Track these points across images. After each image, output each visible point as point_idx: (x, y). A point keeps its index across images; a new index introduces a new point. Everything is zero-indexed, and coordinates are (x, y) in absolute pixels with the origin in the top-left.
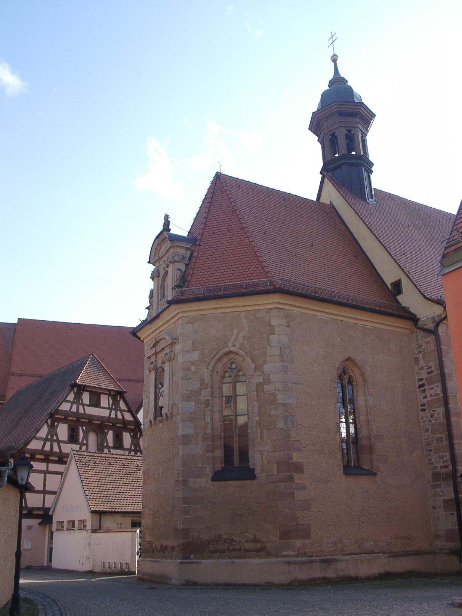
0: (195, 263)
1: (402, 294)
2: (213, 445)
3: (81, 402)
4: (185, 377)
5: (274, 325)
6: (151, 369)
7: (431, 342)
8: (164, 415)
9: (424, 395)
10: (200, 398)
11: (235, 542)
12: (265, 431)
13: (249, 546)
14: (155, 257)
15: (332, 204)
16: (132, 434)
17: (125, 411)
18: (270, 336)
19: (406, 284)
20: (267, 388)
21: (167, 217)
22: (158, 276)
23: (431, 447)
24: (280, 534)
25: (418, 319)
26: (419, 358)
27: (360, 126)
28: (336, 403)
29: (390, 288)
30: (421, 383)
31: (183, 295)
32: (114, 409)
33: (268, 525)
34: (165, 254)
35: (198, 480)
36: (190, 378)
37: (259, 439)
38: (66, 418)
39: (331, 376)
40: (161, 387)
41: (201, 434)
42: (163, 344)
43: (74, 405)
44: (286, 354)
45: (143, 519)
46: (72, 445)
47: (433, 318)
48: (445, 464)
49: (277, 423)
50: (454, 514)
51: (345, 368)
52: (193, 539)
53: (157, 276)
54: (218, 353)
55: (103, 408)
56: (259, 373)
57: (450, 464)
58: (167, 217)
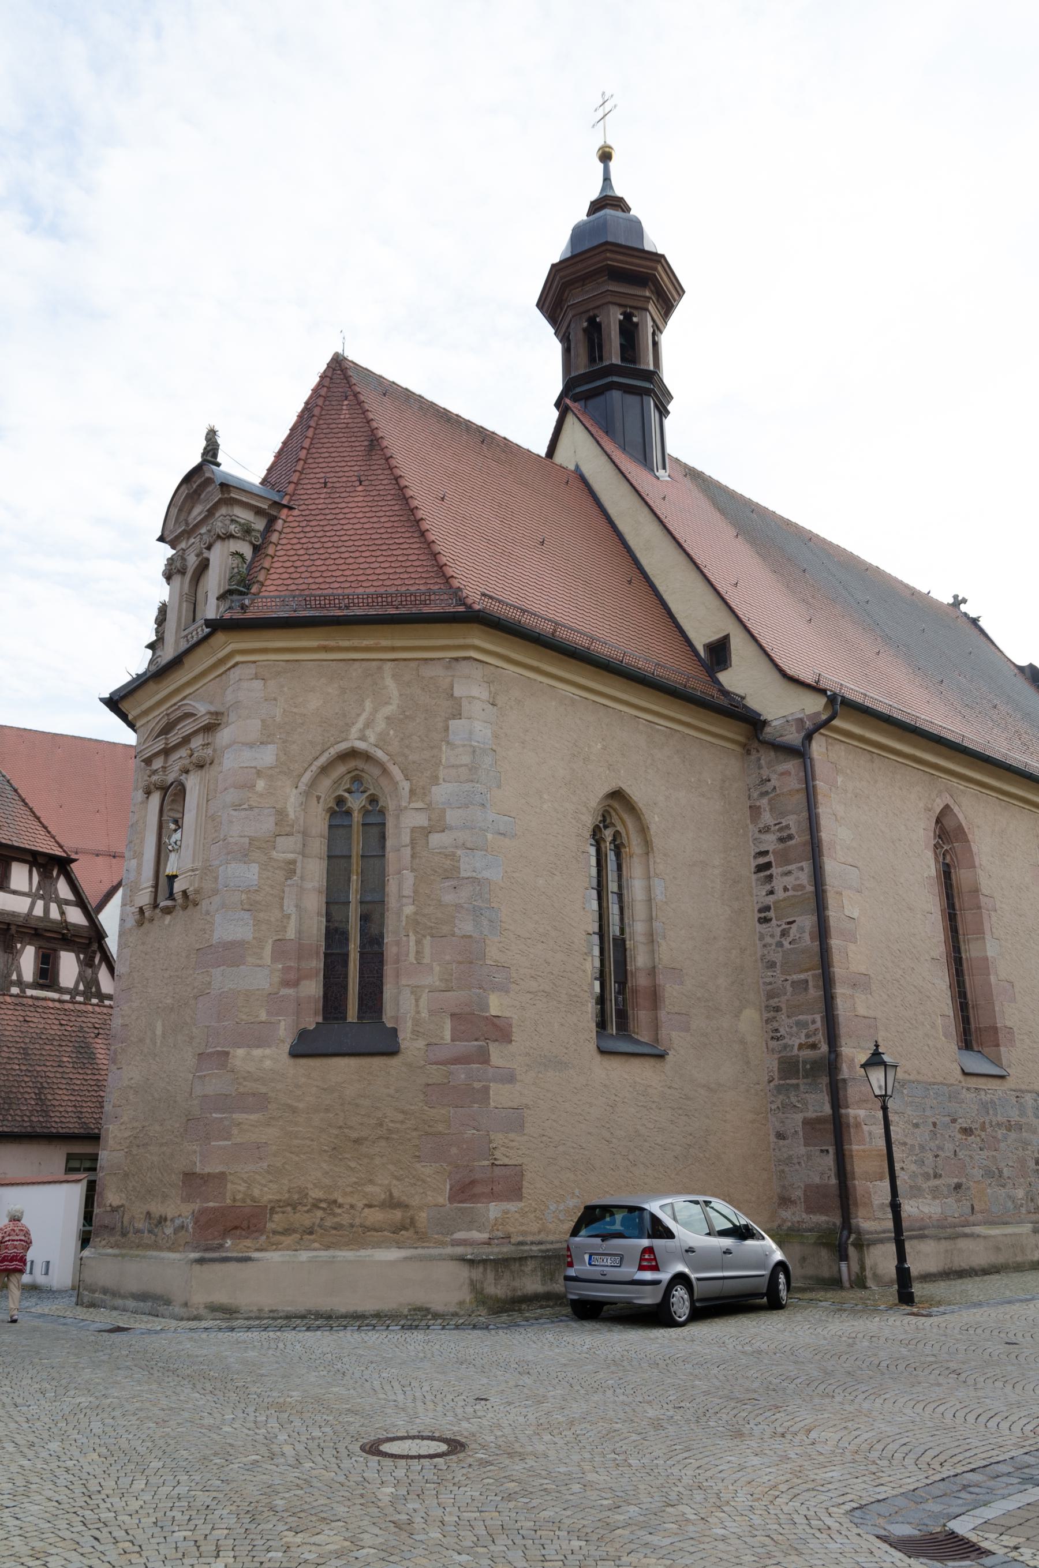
0: (280, 533)
1: (729, 669)
2: (299, 969)
4: (240, 806)
5: (461, 698)
6: (152, 787)
7: (793, 772)
8: (178, 896)
9: (768, 887)
10: (274, 854)
11: (340, 1206)
12: (427, 941)
13: (375, 1216)
14: (177, 525)
15: (580, 470)
16: (82, 956)
17: (67, 902)
18: (451, 722)
19: (739, 646)
20: (435, 839)
21: (211, 437)
22: (182, 572)
23: (779, 1002)
24: (451, 1189)
25: (765, 723)
26: (759, 807)
27: (651, 307)
28: (587, 889)
29: (702, 653)
30: (762, 860)
31: (245, 612)
32: (42, 897)
33: (423, 1166)
34: (202, 520)
35: (257, 1052)
36: (251, 808)
37: (412, 958)
39: (580, 826)
40: (175, 830)
41: (270, 941)
42: (187, 727)
44: (485, 766)
45: (104, 1149)
47: (801, 721)
48: (811, 1040)
49: (456, 921)
50: (827, 1151)
51: (606, 815)
52: (234, 1200)
53: (179, 571)
55: (15, 892)
56: (420, 805)
57: (822, 1040)
58: (211, 437)
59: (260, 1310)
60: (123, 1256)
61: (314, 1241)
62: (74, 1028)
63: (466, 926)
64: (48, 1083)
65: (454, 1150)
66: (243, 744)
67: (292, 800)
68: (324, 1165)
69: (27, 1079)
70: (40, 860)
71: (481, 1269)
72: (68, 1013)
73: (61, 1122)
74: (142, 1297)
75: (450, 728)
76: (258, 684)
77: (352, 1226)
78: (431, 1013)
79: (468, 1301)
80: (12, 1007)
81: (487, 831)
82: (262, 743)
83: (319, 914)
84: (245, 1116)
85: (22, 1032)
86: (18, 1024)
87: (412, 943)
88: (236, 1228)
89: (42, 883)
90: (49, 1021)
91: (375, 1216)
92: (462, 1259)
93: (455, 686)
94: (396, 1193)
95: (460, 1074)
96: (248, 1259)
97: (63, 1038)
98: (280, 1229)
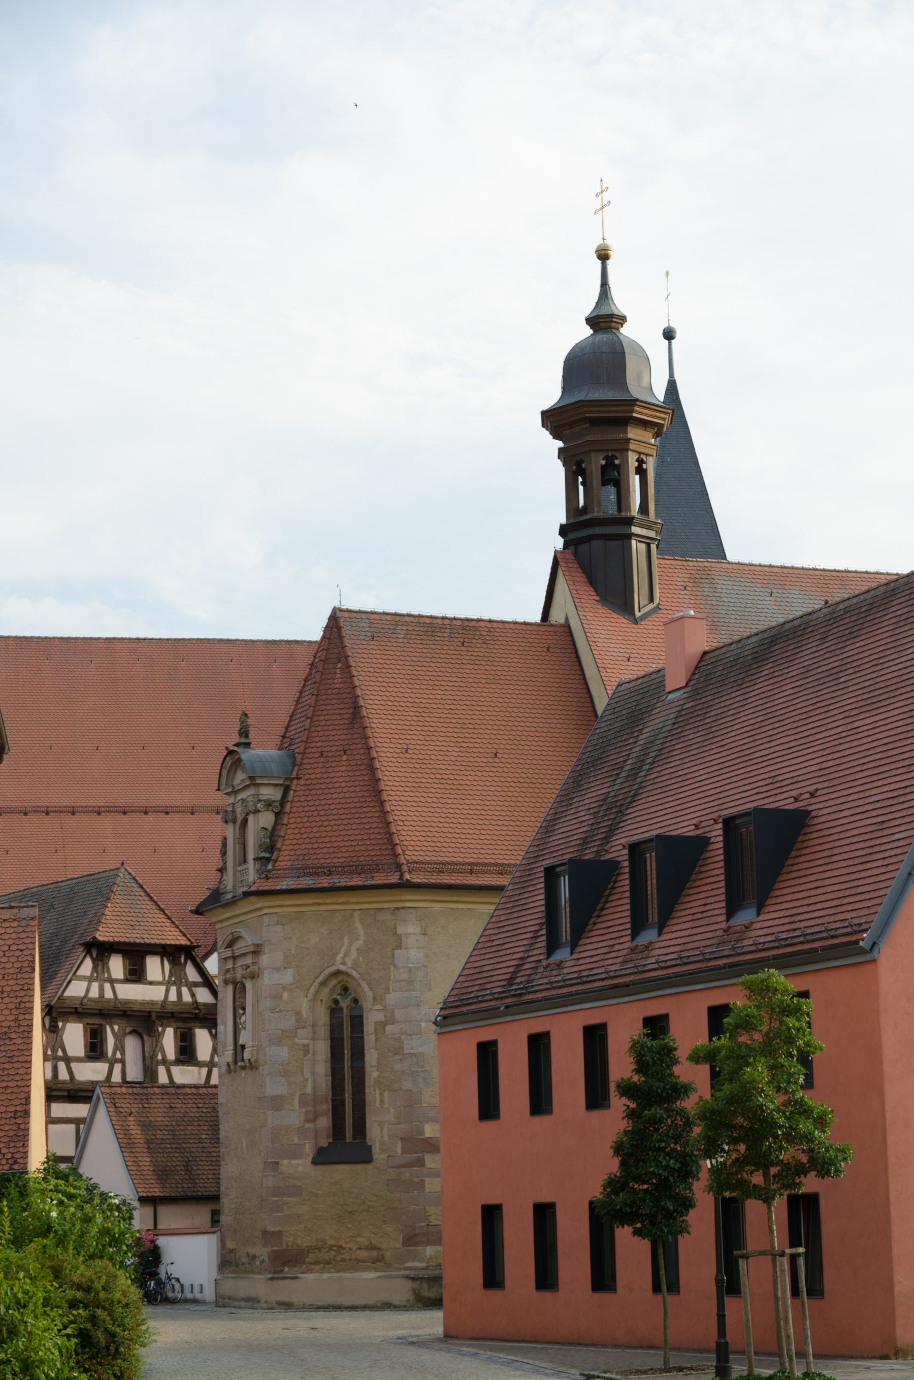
2: (315, 1112)
3: (106, 975)
10: (296, 1040)
11: (344, 1249)
12: (386, 1094)
13: (363, 1254)
17: (196, 985)
20: (390, 1029)
32: (174, 983)
35: (294, 1162)
36: (281, 1011)
37: (378, 1104)
38: (78, 1011)
41: (297, 1095)
43: (93, 983)
46: (93, 1064)
52: (288, 1246)
54: (321, 973)
56: (379, 1007)
59: (304, 1305)
60: (236, 1278)
61: (331, 1268)
62: (209, 1110)
63: (408, 1084)
64: (193, 1157)
65: (404, 1217)
66: (274, 969)
67: (304, 1006)
68: (334, 1226)
69: (177, 1155)
70: (169, 950)
71: (418, 1282)
72: (202, 1097)
73: (205, 1187)
74: (247, 1300)
75: (396, 956)
76: (279, 928)
77: (351, 1260)
78: (390, 1137)
79: (411, 1298)
80: (160, 1097)
81: (421, 1021)
82: (284, 968)
83: (326, 1076)
84: (290, 1199)
85: (169, 1117)
86: (166, 1110)
87: (378, 1095)
88: (289, 1261)
89: (172, 970)
90: (189, 1106)
91: (363, 1254)
92: (408, 1277)
93: (398, 926)
94: (373, 1242)
95: (407, 1173)
96: (296, 1278)
97: (200, 1118)
98: (313, 1262)
